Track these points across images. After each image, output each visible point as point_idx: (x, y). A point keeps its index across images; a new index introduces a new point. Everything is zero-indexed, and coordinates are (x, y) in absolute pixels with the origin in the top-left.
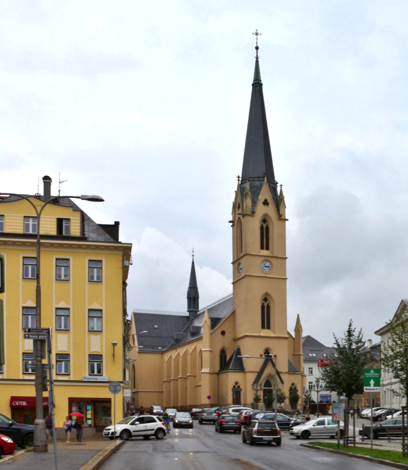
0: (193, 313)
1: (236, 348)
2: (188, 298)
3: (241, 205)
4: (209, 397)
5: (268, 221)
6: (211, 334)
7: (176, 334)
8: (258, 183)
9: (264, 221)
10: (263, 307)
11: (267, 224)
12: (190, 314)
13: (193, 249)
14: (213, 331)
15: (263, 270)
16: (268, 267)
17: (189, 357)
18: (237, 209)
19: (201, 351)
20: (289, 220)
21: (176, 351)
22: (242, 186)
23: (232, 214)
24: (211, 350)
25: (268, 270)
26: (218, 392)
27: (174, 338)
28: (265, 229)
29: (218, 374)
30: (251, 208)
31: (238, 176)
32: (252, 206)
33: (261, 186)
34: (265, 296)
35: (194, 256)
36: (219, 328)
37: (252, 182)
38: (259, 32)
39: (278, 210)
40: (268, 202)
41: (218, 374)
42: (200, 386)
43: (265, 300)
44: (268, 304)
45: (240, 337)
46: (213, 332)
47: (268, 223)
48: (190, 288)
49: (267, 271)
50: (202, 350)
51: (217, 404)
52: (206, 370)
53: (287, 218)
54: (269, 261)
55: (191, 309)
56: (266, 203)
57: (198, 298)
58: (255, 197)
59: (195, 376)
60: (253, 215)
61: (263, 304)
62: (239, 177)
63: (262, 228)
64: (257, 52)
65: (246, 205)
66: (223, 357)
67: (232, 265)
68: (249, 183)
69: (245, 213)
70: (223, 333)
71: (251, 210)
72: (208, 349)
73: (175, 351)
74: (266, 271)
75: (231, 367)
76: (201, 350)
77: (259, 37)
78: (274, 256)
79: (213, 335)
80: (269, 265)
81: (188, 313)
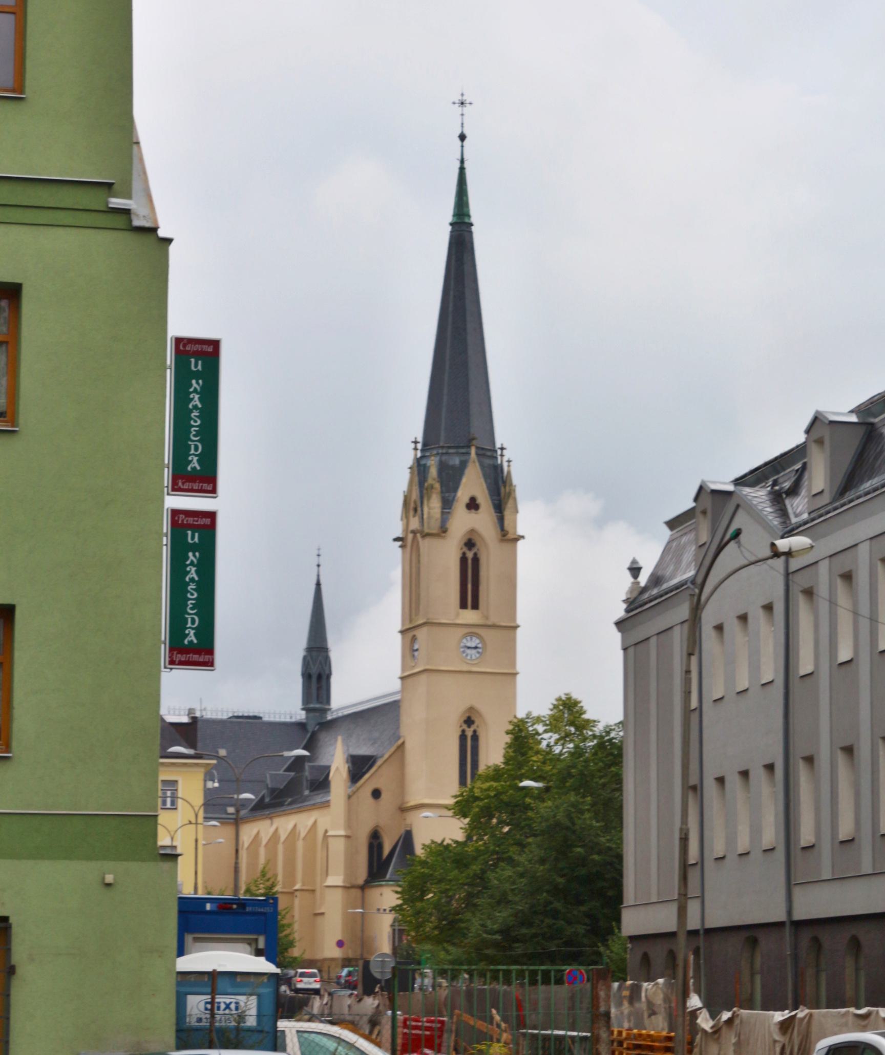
0: (317, 714)
1: (402, 831)
2: (303, 675)
3: (419, 509)
4: (340, 944)
5: (478, 544)
6: (350, 797)
7: (271, 775)
8: (456, 461)
9: (470, 544)
10: (463, 737)
11: (474, 550)
12: (307, 718)
13: (319, 549)
14: (354, 788)
15: (464, 655)
16: (476, 648)
17: (300, 845)
18: (411, 513)
19: (326, 836)
20: (526, 536)
21: (272, 824)
22: (423, 462)
23: (402, 519)
24: (349, 834)
25: (475, 656)
26: (363, 931)
27: (267, 785)
28: (470, 562)
29: (363, 888)
30: (439, 521)
31: (414, 440)
32: (443, 513)
33: (464, 465)
34: (467, 715)
35: (321, 568)
36: (369, 782)
37: (444, 458)
38: (467, 98)
39: (501, 520)
40: (477, 502)
41: (363, 888)
42: (322, 914)
43: (469, 722)
44: (475, 732)
45: (411, 806)
46: (354, 793)
47: (478, 550)
48: (310, 649)
49: (474, 657)
50: (329, 833)
51: (359, 957)
52: (336, 879)
53: (520, 532)
54: (478, 636)
55: (312, 706)
56: (473, 505)
57: (329, 676)
58: (448, 491)
59: (313, 891)
60: (444, 535)
61: (463, 731)
62: (416, 442)
63: (463, 560)
64: (462, 146)
65: (429, 513)
66: (375, 849)
67: (399, 636)
68: (438, 458)
69: (426, 530)
70: (376, 794)
71: (438, 524)
72: (342, 833)
73: (268, 822)
74: (471, 657)
75: (391, 875)
76: (326, 831)
77: (467, 109)
78: (490, 623)
79: (354, 798)
80: (479, 644)
81: (304, 712)
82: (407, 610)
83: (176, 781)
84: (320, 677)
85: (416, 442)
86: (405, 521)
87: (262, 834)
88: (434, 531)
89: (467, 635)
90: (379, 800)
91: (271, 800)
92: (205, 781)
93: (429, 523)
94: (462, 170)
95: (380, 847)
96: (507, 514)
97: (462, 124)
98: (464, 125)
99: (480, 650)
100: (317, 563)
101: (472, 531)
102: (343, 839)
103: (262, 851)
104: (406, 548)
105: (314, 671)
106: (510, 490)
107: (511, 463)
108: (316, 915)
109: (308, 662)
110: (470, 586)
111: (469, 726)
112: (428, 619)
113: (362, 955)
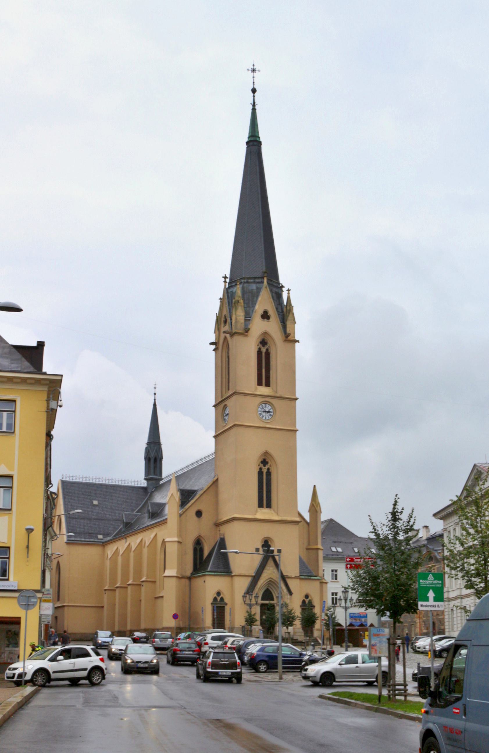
0: (154, 482)
1: (218, 539)
2: (145, 459)
4: (175, 616)
6: (181, 515)
9: (263, 343)
10: (260, 473)
12: (148, 484)
14: (184, 510)
15: (261, 416)
16: (269, 412)
18: (222, 324)
21: (126, 542)
23: (215, 332)
24: (180, 540)
26: (190, 608)
28: (264, 354)
29: (190, 578)
31: (224, 276)
32: (245, 320)
33: (259, 290)
34: (263, 457)
36: (193, 506)
39: (284, 327)
41: (190, 578)
42: (162, 597)
43: (264, 462)
44: (268, 469)
45: (225, 521)
46: (184, 513)
47: (269, 347)
49: (267, 418)
50: (166, 540)
52: (171, 572)
53: (297, 338)
56: (265, 316)
57: (161, 459)
60: (247, 334)
61: (261, 469)
62: (225, 277)
64: (254, 96)
65: (236, 319)
67: (214, 409)
70: (199, 514)
71: (243, 326)
73: (124, 541)
74: (266, 418)
75: (211, 568)
76: (164, 540)
77: (257, 74)
78: (278, 395)
80: (271, 409)
82: (219, 391)
83: (15, 401)
84: (155, 460)
85: (225, 277)
86: (217, 332)
87: (120, 548)
88: (240, 331)
89: (263, 403)
90: (201, 518)
91: (131, 662)
92: (48, 401)
93: (236, 326)
94: (254, 110)
95: (202, 551)
96: (289, 324)
97: (254, 83)
98: (255, 84)
99: (272, 414)
100: (154, 393)
101: (266, 333)
102: (176, 544)
103: (120, 559)
104: (218, 349)
105: (152, 455)
106: (290, 308)
107: (290, 292)
108: (156, 598)
109: (149, 450)
110: (264, 371)
111: (265, 466)
112: (236, 390)
113: (189, 625)
